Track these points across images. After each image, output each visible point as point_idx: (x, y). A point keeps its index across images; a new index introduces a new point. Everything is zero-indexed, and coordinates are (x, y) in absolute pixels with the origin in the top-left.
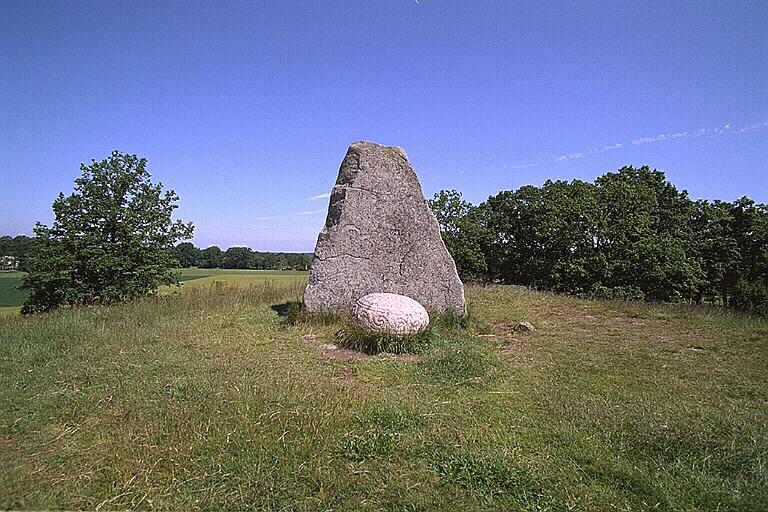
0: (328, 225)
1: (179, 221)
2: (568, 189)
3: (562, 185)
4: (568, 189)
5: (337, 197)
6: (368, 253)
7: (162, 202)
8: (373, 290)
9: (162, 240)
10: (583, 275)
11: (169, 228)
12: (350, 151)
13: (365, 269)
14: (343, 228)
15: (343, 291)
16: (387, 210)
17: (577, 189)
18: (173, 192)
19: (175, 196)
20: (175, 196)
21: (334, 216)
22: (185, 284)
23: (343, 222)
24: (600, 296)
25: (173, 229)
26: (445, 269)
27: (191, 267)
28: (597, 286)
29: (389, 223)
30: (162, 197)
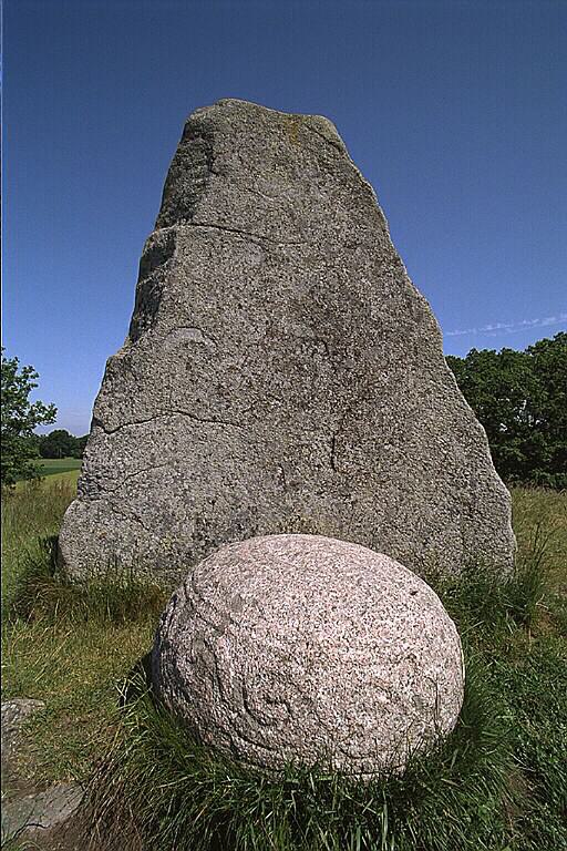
0: (134, 335)
1: (39, 403)
2: (496, 360)
3: (489, 355)
4: (496, 360)
5: (156, 258)
6: (240, 404)
7: (19, 380)
8: (244, 527)
9: (17, 425)
10: (520, 459)
11: (27, 411)
12: (190, 132)
13: (230, 456)
14: (171, 336)
15: (168, 520)
16: (290, 287)
17: (507, 358)
18: (31, 368)
19: (33, 373)
20: (33, 373)
21: (148, 303)
22: (50, 479)
23: (165, 322)
24: (541, 482)
25: (32, 413)
26: (460, 452)
27: (66, 458)
28: (537, 472)
29: (300, 320)
30: (18, 374)
